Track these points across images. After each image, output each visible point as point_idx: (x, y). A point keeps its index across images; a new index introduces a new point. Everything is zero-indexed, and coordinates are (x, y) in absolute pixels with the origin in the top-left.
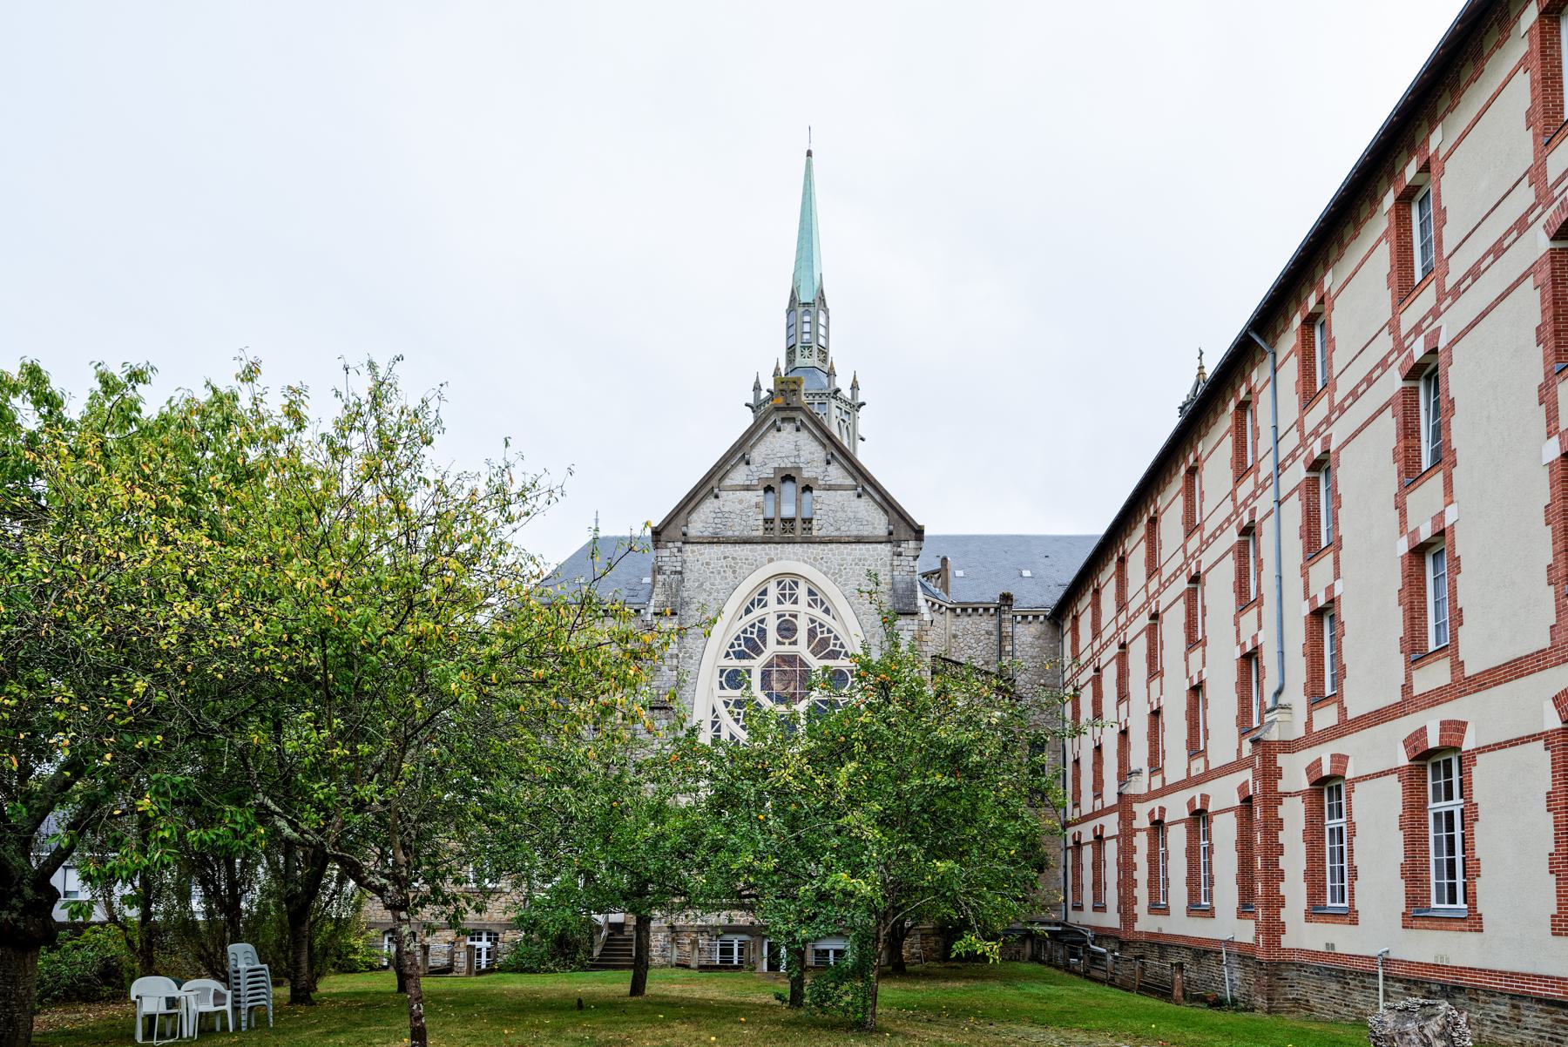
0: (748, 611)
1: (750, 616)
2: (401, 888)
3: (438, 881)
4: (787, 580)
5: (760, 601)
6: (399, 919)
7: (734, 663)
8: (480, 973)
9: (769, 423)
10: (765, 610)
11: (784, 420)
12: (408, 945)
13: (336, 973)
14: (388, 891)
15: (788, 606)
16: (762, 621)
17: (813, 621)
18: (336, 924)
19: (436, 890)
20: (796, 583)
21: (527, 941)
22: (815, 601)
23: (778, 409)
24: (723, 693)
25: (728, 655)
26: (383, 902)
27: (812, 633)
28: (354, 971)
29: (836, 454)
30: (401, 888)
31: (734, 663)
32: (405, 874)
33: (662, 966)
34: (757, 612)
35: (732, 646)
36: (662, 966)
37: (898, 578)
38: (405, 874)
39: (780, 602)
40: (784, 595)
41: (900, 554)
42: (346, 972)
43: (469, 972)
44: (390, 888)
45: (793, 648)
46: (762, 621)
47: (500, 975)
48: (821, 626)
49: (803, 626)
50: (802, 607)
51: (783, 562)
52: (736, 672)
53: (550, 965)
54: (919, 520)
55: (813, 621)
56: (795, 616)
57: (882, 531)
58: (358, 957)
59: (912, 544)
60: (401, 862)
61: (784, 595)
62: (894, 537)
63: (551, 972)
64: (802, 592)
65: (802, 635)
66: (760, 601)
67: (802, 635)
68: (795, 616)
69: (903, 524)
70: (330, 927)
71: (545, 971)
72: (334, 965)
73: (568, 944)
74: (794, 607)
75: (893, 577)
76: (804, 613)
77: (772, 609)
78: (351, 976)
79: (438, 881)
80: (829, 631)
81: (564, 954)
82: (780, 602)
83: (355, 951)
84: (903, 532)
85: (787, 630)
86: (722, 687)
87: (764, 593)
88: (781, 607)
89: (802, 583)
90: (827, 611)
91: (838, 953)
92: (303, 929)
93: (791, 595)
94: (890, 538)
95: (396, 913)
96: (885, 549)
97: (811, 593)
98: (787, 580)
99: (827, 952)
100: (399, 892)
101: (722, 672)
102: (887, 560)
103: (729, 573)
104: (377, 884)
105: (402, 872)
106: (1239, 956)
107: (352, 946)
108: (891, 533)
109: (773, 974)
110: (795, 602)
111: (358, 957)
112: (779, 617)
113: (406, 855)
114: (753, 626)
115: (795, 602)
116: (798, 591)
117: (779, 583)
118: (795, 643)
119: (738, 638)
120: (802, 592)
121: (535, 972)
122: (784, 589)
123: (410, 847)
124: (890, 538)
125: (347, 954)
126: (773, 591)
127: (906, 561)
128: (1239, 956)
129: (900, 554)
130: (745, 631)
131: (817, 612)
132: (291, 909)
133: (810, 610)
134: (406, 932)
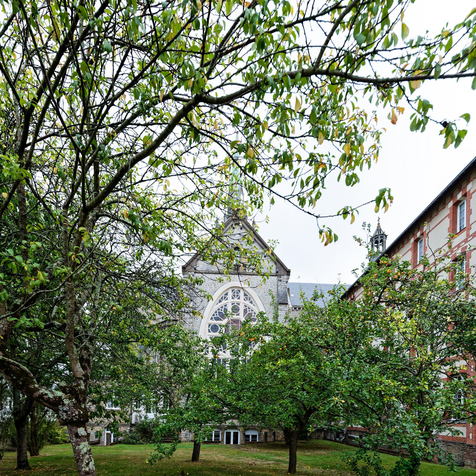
0: (220, 301)
1: (221, 303)
2: (79, 402)
3: (102, 402)
4: (236, 290)
5: (225, 297)
6: (77, 435)
7: (214, 322)
8: (112, 444)
9: (229, 226)
10: (227, 301)
11: (236, 224)
12: (88, 464)
13: (50, 445)
14: (64, 405)
15: (236, 300)
16: (226, 306)
17: (246, 306)
18: (48, 425)
19: (100, 409)
20: (239, 291)
21: (131, 431)
22: (247, 298)
23: (233, 220)
24: (210, 334)
25: (212, 318)
26: (58, 417)
27: (245, 311)
28: (58, 443)
29: (256, 239)
30: (79, 402)
31: (214, 322)
32: (83, 387)
33: (186, 441)
34: (224, 302)
35: (214, 315)
36: (186, 441)
37: (280, 290)
38: (83, 387)
39: (233, 298)
40: (234, 296)
41: (281, 281)
42: (54, 444)
43: (107, 444)
44: (66, 402)
45: (238, 317)
46: (226, 306)
47: (124, 445)
48: (249, 308)
49: (242, 308)
50: (242, 300)
51: (235, 282)
52: (238, 310)
53: (141, 441)
54: (289, 267)
55: (246, 306)
56: (239, 304)
57: (274, 271)
58: (59, 438)
59: (286, 277)
60: (79, 375)
61: (234, 296)
62: (279, 273)
63: (142, 444)
64: (242, 294)
65: (241, 312)
66: (225, 297)
67: (241, 312)
68: (239, 304)
69: (282, 269)
70: (45, 426)
71: (139, 444)
72: (49, 441)
73: (148, 432)
74: (238, 300)
75: (278, 290)
76: (242, 303)
77: (230, 300)
78: (56, 446)
79: (102, 402)
80: (252, 310)
81: (146, 437)
82: (233, 298)
83: (58, 435)
84: (282, 272)
85: (235, 309)
86: (209, 332)
87: (227, 294)
88: (233, 300)
89: (242, 291)
90: (251, 302)
91: (254, 437)
92: (24, 429)
93: (237, 296)
94: (277, 274)
95: (74, 429)
96: (275, 278)
97: (245, 295)
98: (236, 290)
99: (249, 436)
100: (77, 405)
101: (209, 325)
102: (276, 283)
103: (213, 286)
104: (51, 396)
105: (79, 385)
106: (443, 441)
107: (57, 433)
108: (277, 272)
109: (228, 445)
110: (239, 298)
111: (59, 438)
112: (232, 304)
113: (84, 368)
114: (222, 307)
115: (239, 298)
116: (240, 294)
117: (233, 291)
118: (238, 315)
119: (216, 312)
120: (242, 294)
121: (134, 444)
122: (234, 293)
123: (88, 361)
124: (277, 274)
125: (55, 436)
126: (230, 294)
127: (283, 284)
128: (443, 441)
129: (281, 281)
130: (219, 309)
131: (248, 303)
132: (17, 419)
133: (244, 302)
134: (85, 450)
